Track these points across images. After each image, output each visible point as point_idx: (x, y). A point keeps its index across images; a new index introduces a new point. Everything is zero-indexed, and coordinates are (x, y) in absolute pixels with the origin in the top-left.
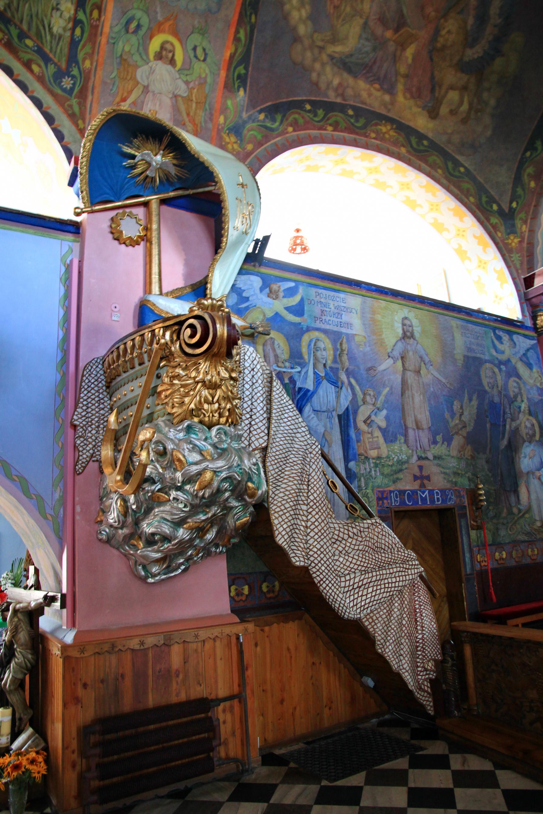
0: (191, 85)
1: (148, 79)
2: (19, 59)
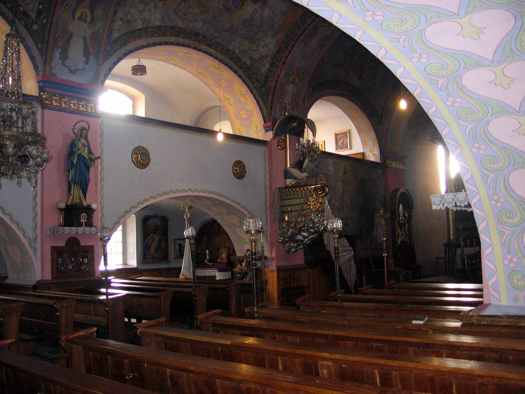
2: (250, 81)
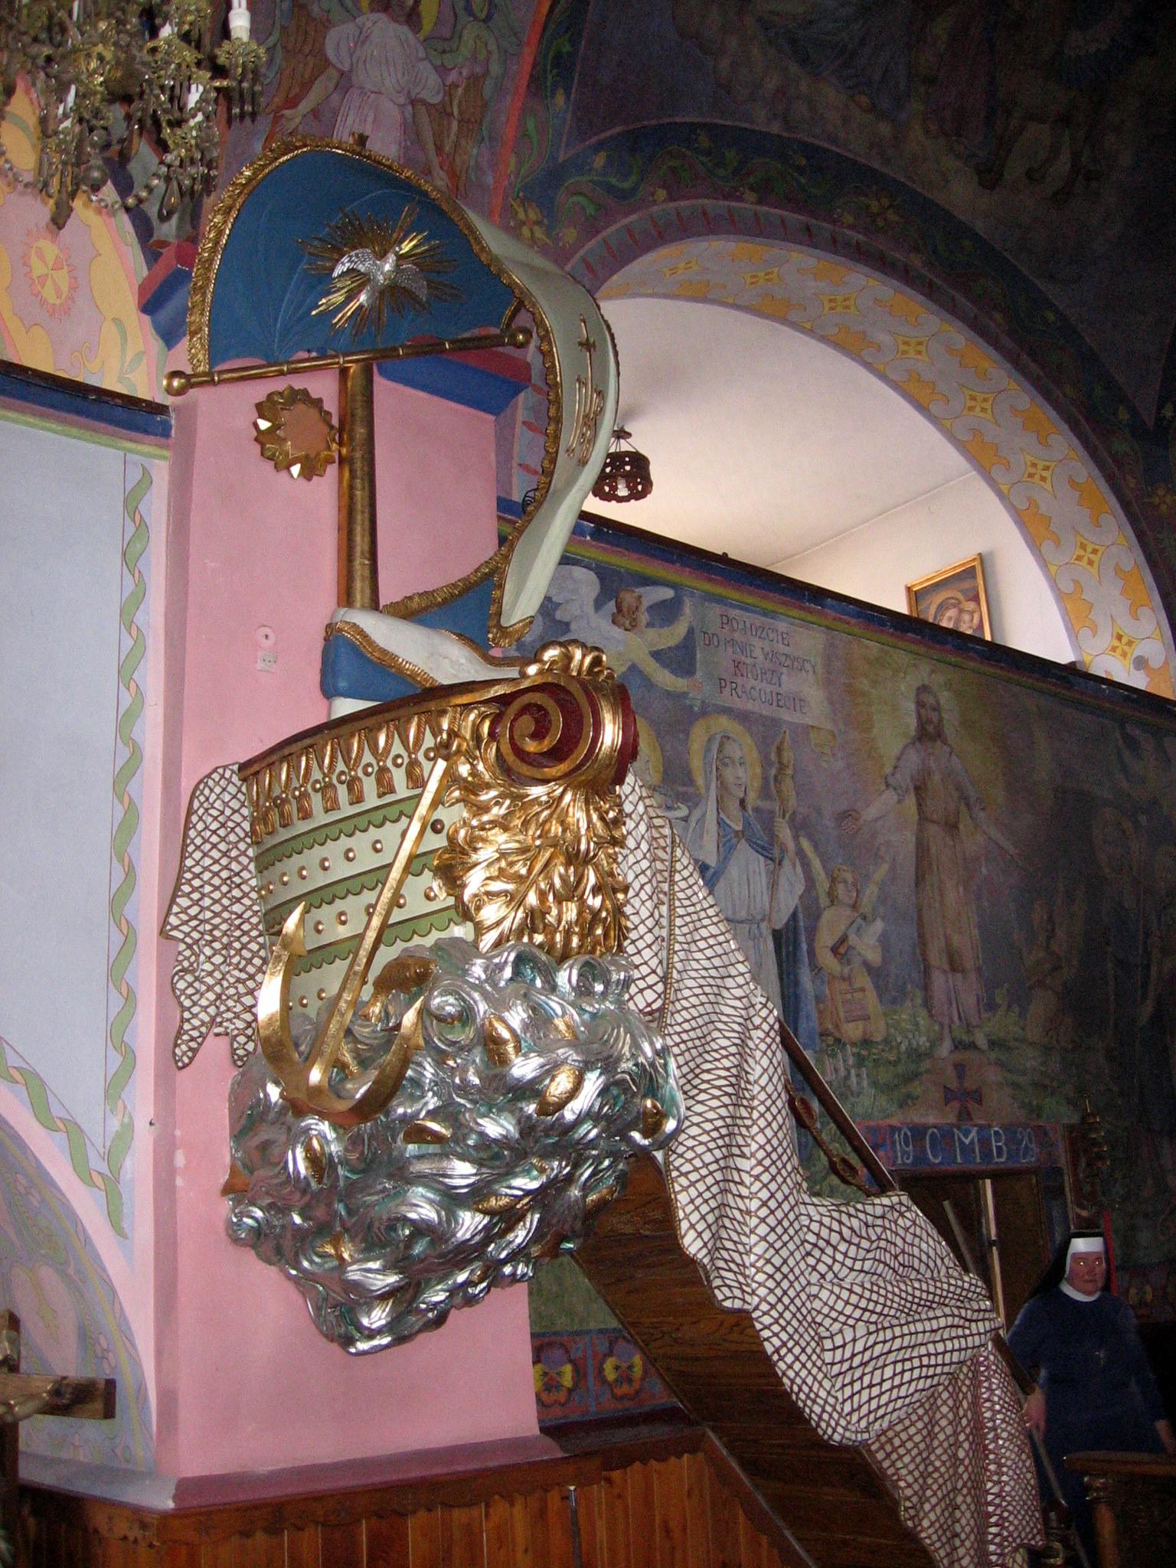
0: (453, 77)
1: (351, 56)
